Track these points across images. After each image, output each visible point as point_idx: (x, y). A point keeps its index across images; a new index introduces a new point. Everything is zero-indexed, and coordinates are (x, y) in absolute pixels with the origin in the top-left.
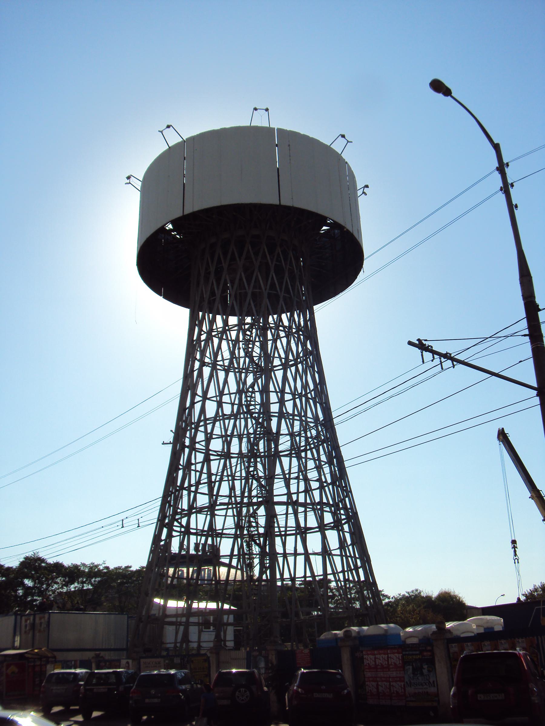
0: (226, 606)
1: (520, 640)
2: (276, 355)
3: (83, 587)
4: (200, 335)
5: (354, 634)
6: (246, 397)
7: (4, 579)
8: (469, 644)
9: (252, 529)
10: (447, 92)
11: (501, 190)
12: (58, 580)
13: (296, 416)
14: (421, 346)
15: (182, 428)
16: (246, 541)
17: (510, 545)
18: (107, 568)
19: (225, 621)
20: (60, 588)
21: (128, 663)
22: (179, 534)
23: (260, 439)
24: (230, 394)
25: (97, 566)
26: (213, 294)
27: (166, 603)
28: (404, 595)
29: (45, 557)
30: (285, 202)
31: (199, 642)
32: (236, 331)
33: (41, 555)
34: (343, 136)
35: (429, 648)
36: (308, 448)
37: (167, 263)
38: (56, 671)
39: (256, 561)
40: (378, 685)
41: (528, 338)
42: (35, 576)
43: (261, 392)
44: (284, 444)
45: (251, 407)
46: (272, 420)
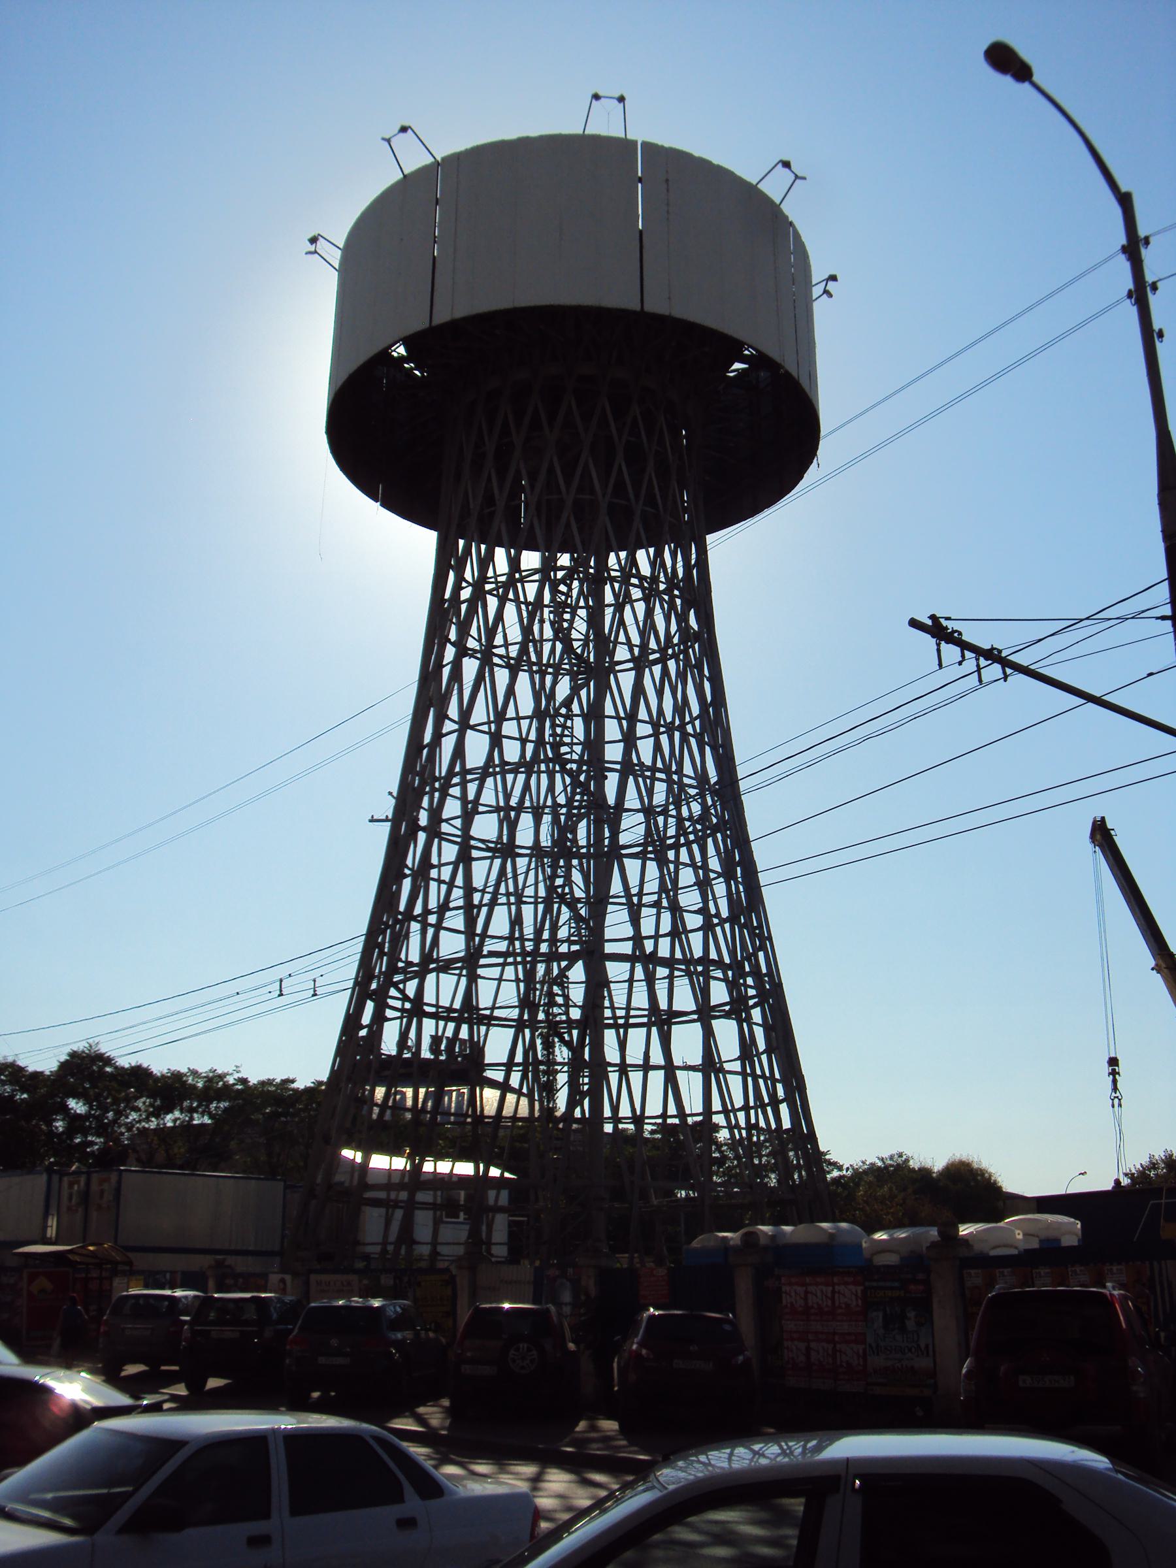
0: (494, 1172)
1: (1115, 1268)
2: (622, 638)
3: (192, 1119)
4: (457, 588)
7: (25, 1096)
9: (556, 1010)
12: (139, 1103)
14: (938, 630)
15: (414, 789)
17: (1106, 1069)
18: (244, 1081)
19: (491, 1201)
20: (143, 1120)
21: (283, 1281)
23: (580, 817)
24: (518, 718)
25: (221, 1077)
26: (490, 500)
28: (873, 1164)
29: (112, 1054)
30: (655, 305)
31: (434, 1243)
33: (105, 1048)
34: (786, 165)
35: (921, 1276)
36: (682, 840)
37: (400, 427)
38: (134, 1291)
39: (562, 1078)
40: (808, 1349)
41: (1169, 623)
42: (91, 1093)
44: (632, 829)
45: (564, 749)
46: (606, 778)
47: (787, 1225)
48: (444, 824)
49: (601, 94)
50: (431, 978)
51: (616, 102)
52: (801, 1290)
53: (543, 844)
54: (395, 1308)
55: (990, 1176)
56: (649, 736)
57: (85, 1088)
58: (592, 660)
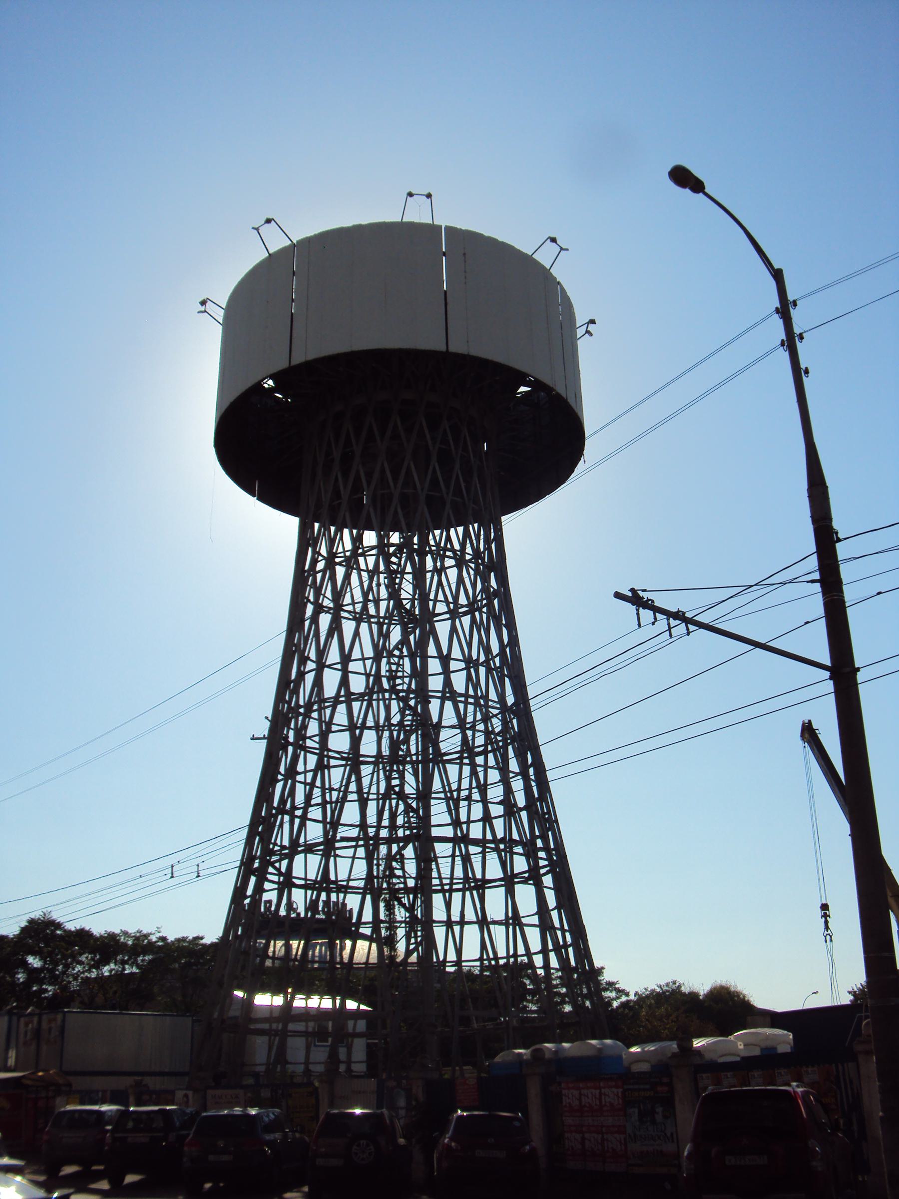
0: (351, 1005)
1: (810, 1069)
2: (441, 597)
3: (124, 969)
4: (314, 562)
5: (547, 1055)
6: (389, 663)
8: (729, 1074)
9: (395, 880)
10: (697, 186)
11: (782, 344)
12: (83, 958)
13: (471, 697)
14: (636, 599)
15: (283, 714)
16: (385, 900)
17: (819, 913)
18: (164, 939)
19: (350, 1030)
20: (86, 971)
21: (186, 1096)
22: (276, 886)
24: (363, 659)
25: (146, 936)
26: (337, 494)
27: (551, 950)
28: (653, 991)
30: (457, 346)
31: (307, 1063)
32: (374, 557)
33: (57, 915)
34: (553, 240)
35: (665, 1080)
36: (490, 748)
37: (261, 443)
38: (70, 1108)
39: (401, 932)
40: (583, 1139)
41: (818, 585)
42: (45, 950)
43: (412, 656)
44: (450, 741)
45: (398, 681)
46: (430, 702)
47: (593, 1039)
48: (308, 741)
49: (413, 192)
50: (299, 859)
51: (425, 197)
52: (576, 1093)
53: (384, 754)
54: (272, 1113)
55: (744, 997)
56: (463, 669)
57: (40, 947)
58: (417, 612)
